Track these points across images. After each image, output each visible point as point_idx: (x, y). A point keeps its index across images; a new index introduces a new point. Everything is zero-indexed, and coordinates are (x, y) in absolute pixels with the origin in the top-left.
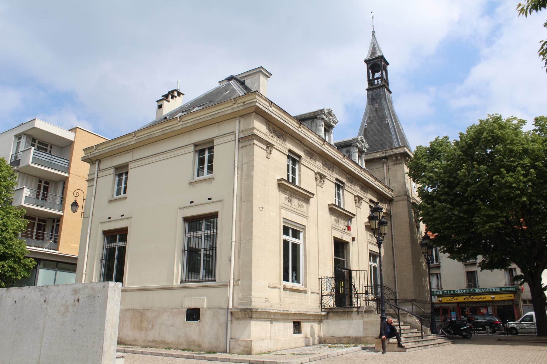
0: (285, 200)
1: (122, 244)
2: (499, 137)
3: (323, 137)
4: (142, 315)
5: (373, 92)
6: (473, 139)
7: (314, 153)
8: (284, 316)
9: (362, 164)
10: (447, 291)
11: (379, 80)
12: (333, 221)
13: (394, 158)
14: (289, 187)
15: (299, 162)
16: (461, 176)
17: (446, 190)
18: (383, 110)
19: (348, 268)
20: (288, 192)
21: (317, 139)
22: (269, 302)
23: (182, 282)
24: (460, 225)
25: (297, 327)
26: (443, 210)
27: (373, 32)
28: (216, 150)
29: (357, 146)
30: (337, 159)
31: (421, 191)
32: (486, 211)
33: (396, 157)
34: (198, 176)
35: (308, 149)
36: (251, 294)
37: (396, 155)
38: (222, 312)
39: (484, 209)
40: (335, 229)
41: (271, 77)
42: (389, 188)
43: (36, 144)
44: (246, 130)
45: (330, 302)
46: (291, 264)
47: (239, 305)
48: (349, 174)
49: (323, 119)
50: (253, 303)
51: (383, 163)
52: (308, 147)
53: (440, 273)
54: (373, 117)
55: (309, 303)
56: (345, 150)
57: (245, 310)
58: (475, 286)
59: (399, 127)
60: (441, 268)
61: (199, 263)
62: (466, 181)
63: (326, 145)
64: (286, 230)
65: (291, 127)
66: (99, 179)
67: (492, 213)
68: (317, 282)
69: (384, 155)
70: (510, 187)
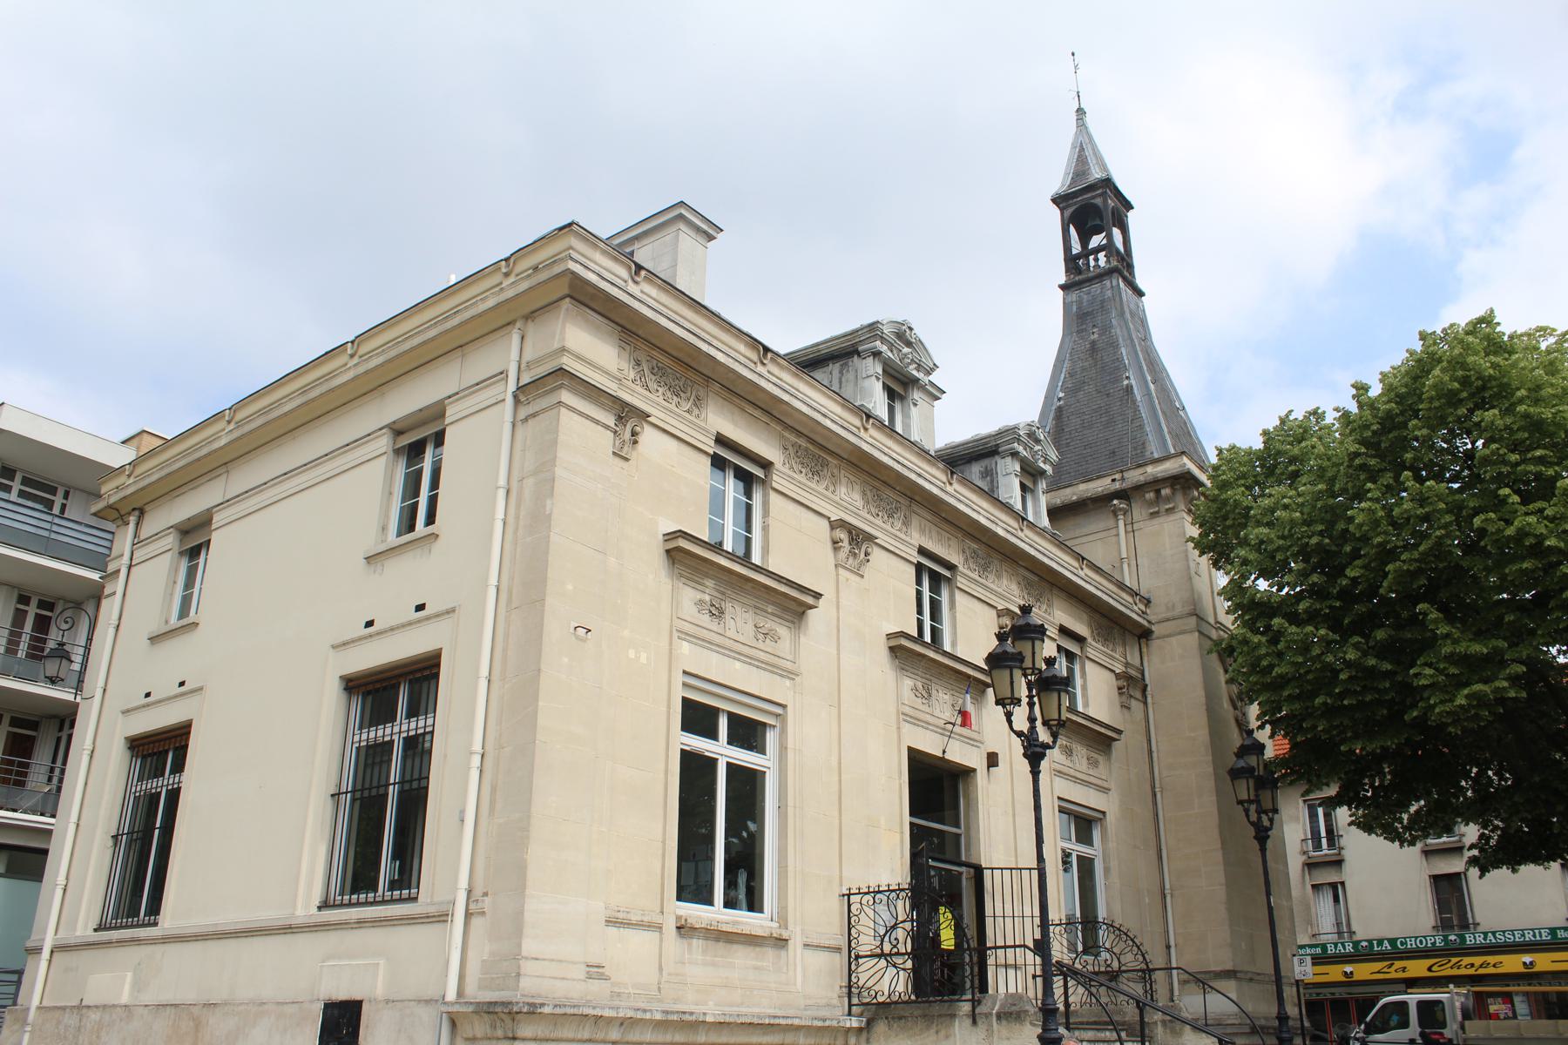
0: (694, 609)
2: (1486, 382)
3: (1018, 506)
4: (198, 1025)
6: (1400, 399)
9: (1037, 513)
10: (1370, 941)
11: (1101, 255)
12: (907, 694)
13: (1150, 495)
16: (1360, 526)
17: (1315, 578)
18: (1114, 345)
19: (974, 861)
20: (710, 583)
21: (838, 409)
22: (603, 977)
24: (1368, 698)
26: (1305, 648)
27: (1080, 112)
29: (1015, 454)
30: (920, 481)
31: (1235, 591)
32: (1456, 642)
33: (1158, 492)
35: (803, 443)
36: (519, 945)
37: (1155, 484)
38: (427, 1015)
39: (1447, 636)
40: (915, 721)
41: (720, 236)
42: (1133, 593)
44: (538, 361)
45: (892, 982)
46: (719, 834)
47: (480, 988)
49: (877, 354)
50: (525, 983)
51: (1115, 514)
52: (799, 434)
53: (1343, 883)
54: (1083, 369)
56: (975, 470)
57: (489, 1010)
58: (1465, 925)
59: (1171, 402)
60: (1346, 866)
61: (381, 834)
62: (1379, 539)
63: (872, 431)
64: (698, 718)
65: (720, 357)
67: (1478, 648)
68: (836, 907)
69: (1117, 486)
70: (1538, 550)
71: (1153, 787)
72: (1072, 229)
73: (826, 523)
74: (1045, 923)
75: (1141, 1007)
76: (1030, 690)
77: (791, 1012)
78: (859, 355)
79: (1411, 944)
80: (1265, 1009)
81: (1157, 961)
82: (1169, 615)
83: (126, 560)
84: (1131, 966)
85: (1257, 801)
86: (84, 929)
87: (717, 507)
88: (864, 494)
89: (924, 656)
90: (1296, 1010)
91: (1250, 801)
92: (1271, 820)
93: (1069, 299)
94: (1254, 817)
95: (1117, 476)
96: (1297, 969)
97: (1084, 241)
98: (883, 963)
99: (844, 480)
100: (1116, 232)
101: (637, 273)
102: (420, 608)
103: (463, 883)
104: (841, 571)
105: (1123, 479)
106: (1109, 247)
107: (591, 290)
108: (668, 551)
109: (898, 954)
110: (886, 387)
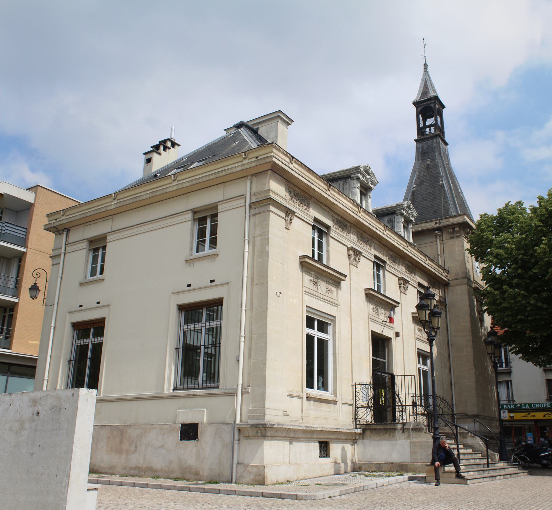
1: (97, 340)
7: (346, 223)
8: (307, 434)
9: (408, 237)
10: (521, 404)
11: (432, 128)
13: (451, 230)
14: (314, 267)
15: (328, 234)
16: (539, 253)
17: (520, 271)
18: (436, 167)
19: (390, 372)
21: (351, 205)
23: (175, 389)
24: (538, 317)
25: (324, 449)
26: (514, 297)
27: (426, 65)
29: (402, 215)
30: (377, 231)
33: (454, 229)
36: (264, 404)
37: (453, 226)
40: (374, 321)
41: (292, 123)
42: (443, 269)
44: (259, 193)
45: (367, 416)
46: (317, 364)
47: (249, 419)
48: (391, 250)
53: (511, 381)
54: (424, 176)
55: (340, 418)
56: (386, 219)
57: (256, 426)
59: (458, 190)
60: (514, 375)
63: (362, 213)
64: (310, 322)
65: (317, 189)
66: (67, 255)
69: (438, 225)
71: (448, 344)
77: (339, 427)
78: (351, 178)
79: (537, 406)
82: (457, 277)
83: (63, 250)
85: (494, 354)
91: (492, 354)
93: (418, 146)
95: (437, 222)
97: (424, 122)
99: (352, 231)
102: (212, 281)
103: (240, 382)
107: (279, 167)
110: (361, 192)
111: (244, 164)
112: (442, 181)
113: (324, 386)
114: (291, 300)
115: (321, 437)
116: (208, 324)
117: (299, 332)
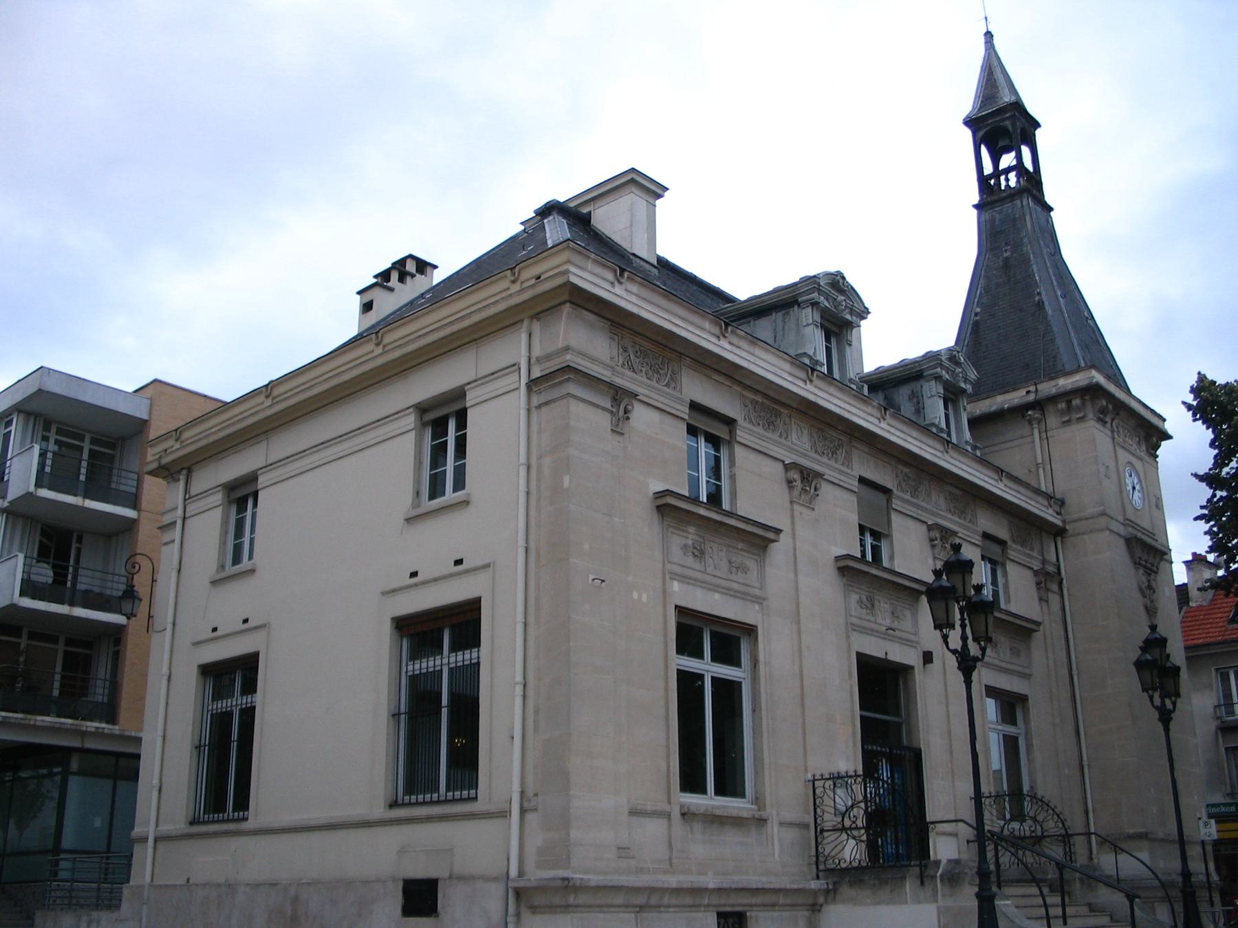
1: (246, 700)
5: (996, 214)
7: (774, 405)
13: (1063, 405)
14: (701, 518)
18: (1025, 261)
19: (915, 745)
20: (692, 530)
23: (193, 823)
27: (989, 35)
28: (471, 415)
29: (938, 378)
33: (1069, 402)
34: (432, 496)
35: (759, 399)
37: (1067, 395)
43: (53, 436)
44: (548, 357)
45: (851, 851)
46: (710, 739)
48: (906, 464)
51: (1030, 423)
52: (756, 392)
66: (188, 522)
69: (1032, 397)
72: (984, 150)
73: (780, 466)
74: (978, 796)
75: (1060, 867)
76: (962, 614)
80: (1169, 864)
81: (1076, 824)
83: (180, 512)
84: (1053, 831)
86: (177, 821)
87: (694, 463)
88: (811, 435)
89: (867, 573)
90: (1201, 867)
92: (1174, 704)
94: (1157, 700)
95: (1032, 388)
96: (1203, 831)
97: (996, 162)
98: (844, 836)
99: (794, 427)
100: (1025, 151)
101: (622, 275)
102: (458, 562)
104: (797, 508)
105: (1037, 391)
106: (1019, 167)
108: (658, 507)
109: (857, 828)
111: (511, 295)
112: (1039, 294)
113: (729, 784)
114: (635, 595)
115: (723, 901)
116: (452, 659)
117: (656, 665)
